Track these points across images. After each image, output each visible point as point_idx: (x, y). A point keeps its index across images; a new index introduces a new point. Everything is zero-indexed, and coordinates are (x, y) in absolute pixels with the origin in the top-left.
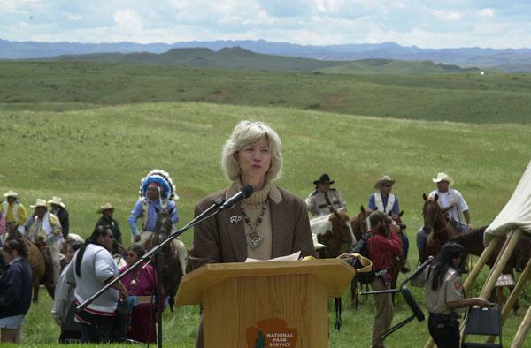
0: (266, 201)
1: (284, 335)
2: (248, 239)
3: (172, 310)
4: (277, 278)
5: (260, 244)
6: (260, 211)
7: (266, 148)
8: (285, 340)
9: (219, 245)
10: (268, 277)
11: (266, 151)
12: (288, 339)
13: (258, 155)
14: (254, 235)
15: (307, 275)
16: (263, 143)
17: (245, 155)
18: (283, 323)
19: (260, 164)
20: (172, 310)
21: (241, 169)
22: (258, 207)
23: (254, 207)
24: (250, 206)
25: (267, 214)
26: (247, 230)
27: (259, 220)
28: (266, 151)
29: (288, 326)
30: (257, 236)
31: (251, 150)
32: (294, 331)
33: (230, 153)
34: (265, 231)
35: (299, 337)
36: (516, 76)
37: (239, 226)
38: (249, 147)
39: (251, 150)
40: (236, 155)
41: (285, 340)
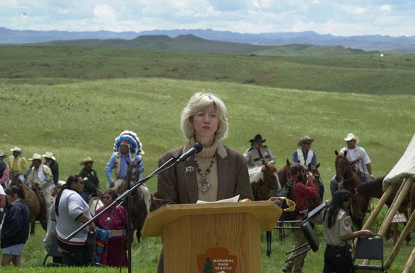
0: (214, 156)
2: (200, 185)
3: (139, 241)
5: (209, 188)
7: (214, 114)
11: (214, 116)
13: (207, 118)
14: (204, 182)
17: (198, 119)
19: (210, 126)
21: (195, 130)
23: (204, 160)
25: (215, 166)
26: (199, 178)
27: (208, 171)
28: (214, 116)
31: (202, 115)
32: (235, 258)
34: (213, 179)
38: (200, 113)
39: (202, 115)
41: (227, 264)
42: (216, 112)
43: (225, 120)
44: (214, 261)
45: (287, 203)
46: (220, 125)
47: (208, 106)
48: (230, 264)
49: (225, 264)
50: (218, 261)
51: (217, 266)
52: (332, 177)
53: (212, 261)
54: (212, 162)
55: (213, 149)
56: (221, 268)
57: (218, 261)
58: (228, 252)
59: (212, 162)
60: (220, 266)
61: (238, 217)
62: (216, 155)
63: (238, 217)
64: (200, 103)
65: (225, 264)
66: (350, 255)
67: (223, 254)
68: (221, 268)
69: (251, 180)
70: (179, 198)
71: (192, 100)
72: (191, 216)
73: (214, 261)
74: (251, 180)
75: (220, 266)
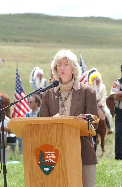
0: (71, 89)
1: (53, 152)
2: (60, 107)
3: (103, 151)
5: (65, 109)
6: (68, 94)
9: (49, 111)
10: (44, 125)
14: (63, 105)
18: (52, 147)
19: (65, 72)
20: (103, 151)
22: (67, 92)
23: (65, 92)
25: (70, 96)
26: (60, 103)
27: (66, 99)
29: (54, 148)
30: (64, 106)
32: (57, 151)
34: (68, 103)
35: (59, 154)
36: (38, 44)
37: (57, 101)
38: (59, 64)
41: (53, 155)
44: (45, 152)
46: (73, 69)
47: (62, 59)
48: (55, 155)
49: (51, 155)
50: (47, 152)
51: (47, 156)
52: (119, 78)
56: (49, 157)
58: (54, 148)
59: (69, 93)
60: (48, 156)
65: (51, 155)
68: (49, 157)
69: (55, 92)
71: (55, 58)
72: (30, 125)
73: (45, 152)
74: (55, 92)
75: (48, 156)
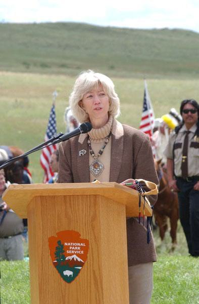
0: (109, 136)
1: (79, 244)
2: (92, 168)
4: (72, 198)
5: (101, 171)
6: (102, 145)
7: (102, 93)
8: (79, 248)
9: (71, 174)
10: (65, 196)
11: (103, 94)
12: (81, 247)
13: (97, 99)
14: (96, 165)
15: (95, 196)
16: (97, 88)
17: (88, 102)
18: (78, 234)
19: (101, 106)
21: (87, 113)
23: (98, 141)
24: (95, 142)
25: (108, 147)
26: (91, 161)
27: (101, 153)
28: (103, 94)
29: (81, 237)
31: (91, 96)
32: (86, 242)
33: (75, 104)
34: (106, 161)
35: (90, 246)
38: (89, 95)
39: (91, 96)
40: (81, 103)
41: (79, 248)
42: (103, 90)
43: (114, 97)
44: (66, 244)
45: (148, 185)
46: (111, 102)
49: (76, 248)
50: (69, 244)
51: (69, 250)
53: (64, 245)
54: (106, 143)
55: (105, 131)
56: (73, 252)
57: (69, 244)
59: (106, 143)
60: (71, 250)
61: (88, 199)
62: (111, 134)
63: (88, 199)
64: (86, 85)
65: (76, 248)
66: (79, 243)
67: (74, 237)
68: (73, 252)
70: (73, 178)
72: (40, 196)
73: (66, 244)
75: (71, 250)
